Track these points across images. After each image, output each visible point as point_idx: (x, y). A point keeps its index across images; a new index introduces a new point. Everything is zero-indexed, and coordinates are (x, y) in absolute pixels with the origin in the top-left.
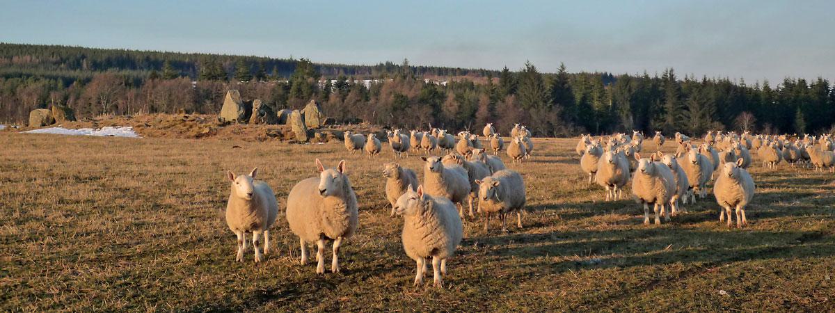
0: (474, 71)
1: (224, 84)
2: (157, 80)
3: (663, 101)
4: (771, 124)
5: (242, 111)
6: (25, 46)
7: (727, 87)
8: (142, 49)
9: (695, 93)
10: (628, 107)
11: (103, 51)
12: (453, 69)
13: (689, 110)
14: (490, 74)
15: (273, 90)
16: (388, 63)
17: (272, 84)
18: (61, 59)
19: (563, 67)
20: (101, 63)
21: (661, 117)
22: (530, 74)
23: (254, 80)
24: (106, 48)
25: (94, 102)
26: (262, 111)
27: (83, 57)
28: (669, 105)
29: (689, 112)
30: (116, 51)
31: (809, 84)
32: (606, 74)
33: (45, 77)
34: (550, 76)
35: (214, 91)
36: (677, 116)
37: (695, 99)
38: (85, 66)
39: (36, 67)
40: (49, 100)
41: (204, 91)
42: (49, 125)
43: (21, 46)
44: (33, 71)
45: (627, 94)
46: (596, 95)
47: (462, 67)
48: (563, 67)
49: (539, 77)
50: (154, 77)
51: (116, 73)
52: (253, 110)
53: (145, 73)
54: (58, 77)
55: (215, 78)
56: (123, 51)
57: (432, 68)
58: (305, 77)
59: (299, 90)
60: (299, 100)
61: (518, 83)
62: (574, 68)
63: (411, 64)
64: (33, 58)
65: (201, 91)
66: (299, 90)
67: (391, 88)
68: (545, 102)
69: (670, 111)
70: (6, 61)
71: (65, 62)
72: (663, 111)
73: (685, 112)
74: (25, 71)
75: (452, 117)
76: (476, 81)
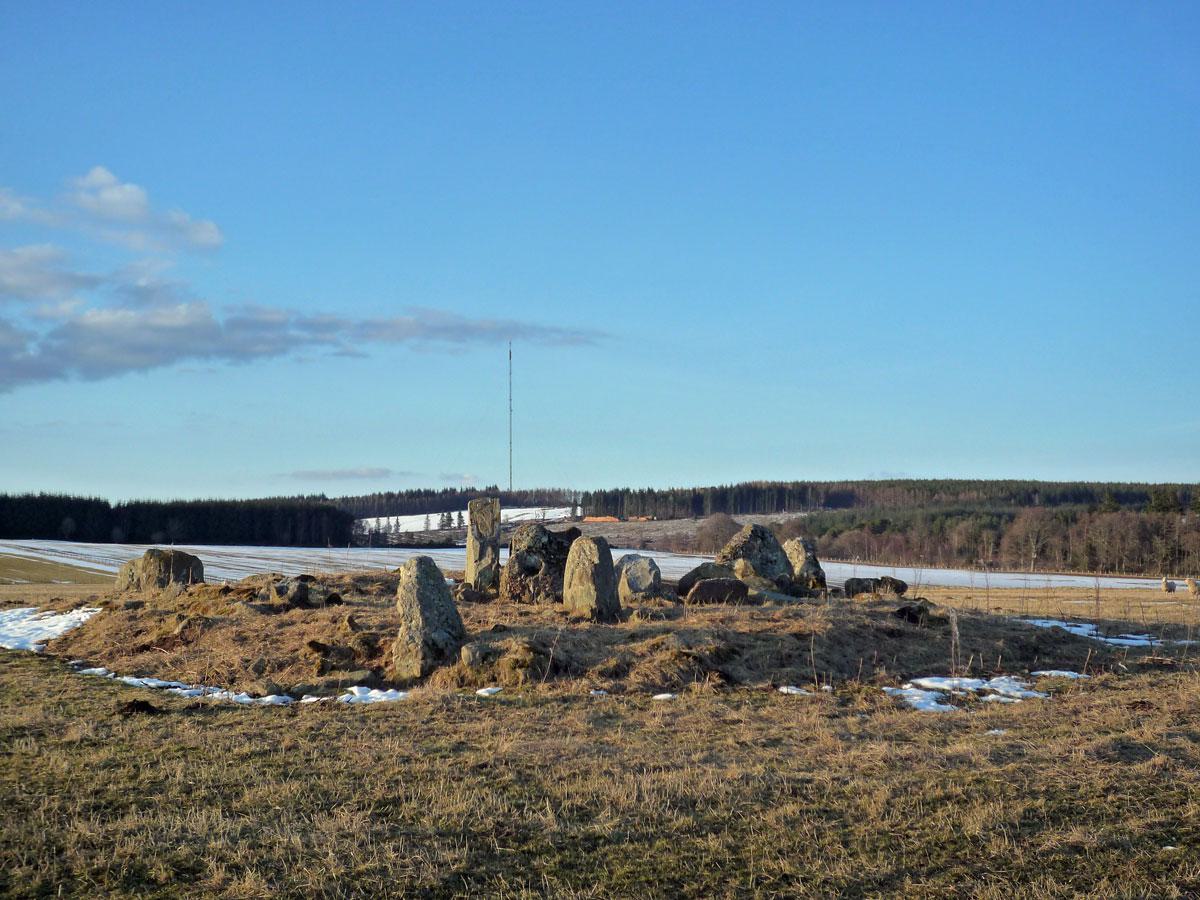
2: (1095, 514)
6: (974, 482)
8: (1104, 480)
11: (1058, 485)
18: (1011, 494)
20: (1055, 498)
25: (1021, 542)
26: (533, 559)
32: (419, 490)
33: (988, 514)
35: (1165, 525)
38: (1037, 501)
39: (982, 504)
40: (980, 539)
41: (1152, 525)
42: (1121, 571)
43: (969, 483)
44: (977, 508)
51: (1070, 508)
53: (1081, 509)
54: (1004, 514)
55: (1166, 509)
56: (1082, 483)
64: (981, 494)
65: (1148, 526)
70: (952, 498)
71: (1015, 497)
74: (969, 509)
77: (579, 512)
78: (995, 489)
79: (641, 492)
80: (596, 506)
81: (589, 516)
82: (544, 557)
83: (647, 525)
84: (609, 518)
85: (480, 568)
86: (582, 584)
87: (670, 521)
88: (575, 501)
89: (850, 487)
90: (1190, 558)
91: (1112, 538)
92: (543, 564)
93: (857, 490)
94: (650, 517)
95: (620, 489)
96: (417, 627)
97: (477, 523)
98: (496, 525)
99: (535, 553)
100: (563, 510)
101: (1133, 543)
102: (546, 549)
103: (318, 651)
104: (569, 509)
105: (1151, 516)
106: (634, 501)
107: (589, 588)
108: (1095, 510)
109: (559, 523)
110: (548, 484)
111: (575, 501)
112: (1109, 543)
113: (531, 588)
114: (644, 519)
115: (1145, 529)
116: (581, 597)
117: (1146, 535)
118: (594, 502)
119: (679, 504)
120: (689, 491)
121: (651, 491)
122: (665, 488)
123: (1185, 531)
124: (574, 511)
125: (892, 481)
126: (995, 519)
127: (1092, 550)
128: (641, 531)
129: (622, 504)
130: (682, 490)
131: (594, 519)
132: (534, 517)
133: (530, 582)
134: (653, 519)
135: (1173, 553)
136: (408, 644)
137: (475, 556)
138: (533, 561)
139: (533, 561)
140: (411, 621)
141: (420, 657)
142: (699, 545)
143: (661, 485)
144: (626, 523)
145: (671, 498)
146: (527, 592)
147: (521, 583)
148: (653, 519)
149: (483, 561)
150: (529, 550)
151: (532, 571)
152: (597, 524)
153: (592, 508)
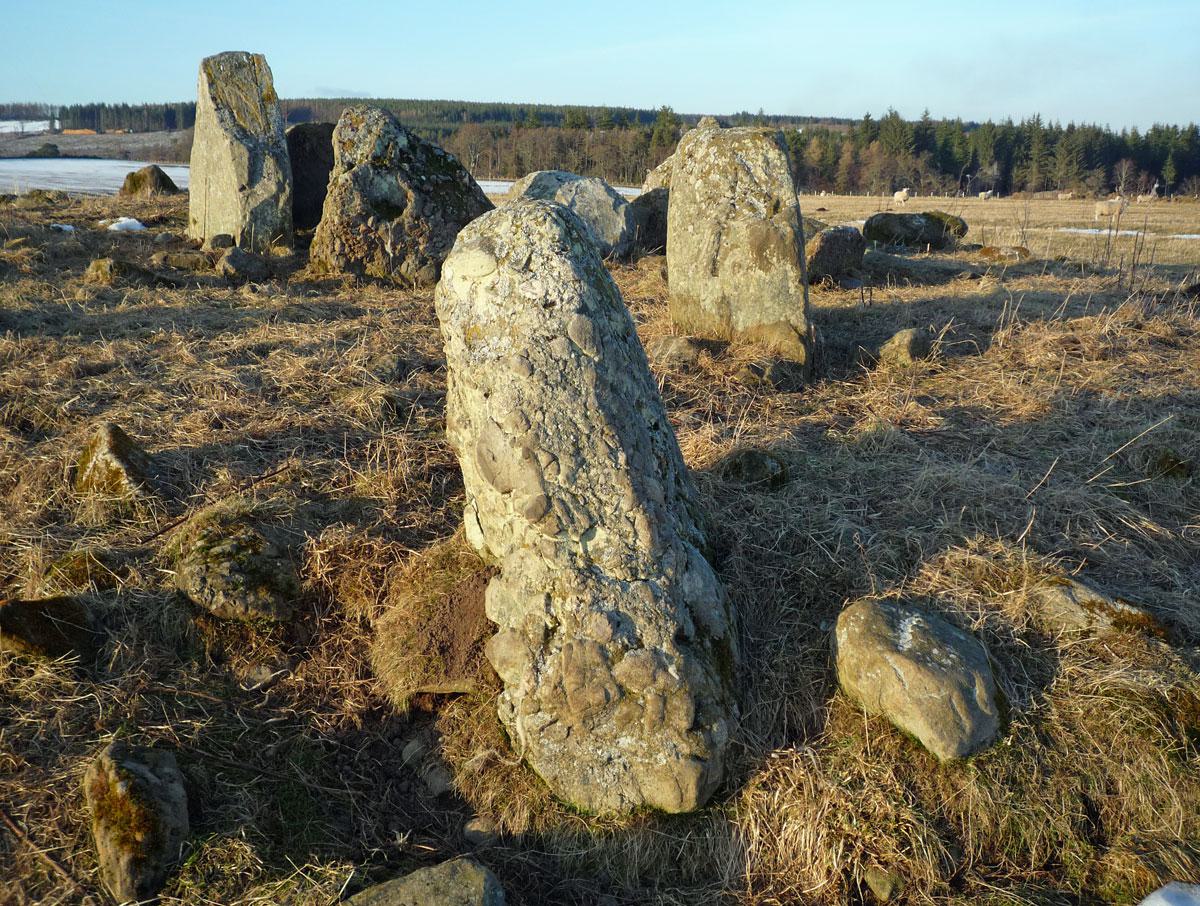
0: (826, 120)
1: (587, 133)
2: (522, 130)
3: (1028, 148)
4: (1147, 173)
5: (266, 188)
6: (412, 101)
7: (1096, 133)
9: (1062, 139)
10: (992, 154)
11: (481, 105)
12: (805, 118)
13: (1054, 156)
14: (852, 123)
15: (635, 138)
16: (744, 113)
17: (633, 132)
19: (927, 113)
21: (1025, 164)
22: (893, 122)
23: (616, 129)
24: (485, 101)
26: (389, 184)
27: (464, 110)
28: (1034, 152)
29: (981, 152)
30: (494, 104)
31: (1180, 129)
33: (427, 129)
34: (911, 124)
36: (1042, 163)
37: (1062, 146)
38: (465, 118)
39: (420, 120)
43: (408, 102)
44: (417, 124)
45: (991, 141)
46: (956, 142)
47: (814, 116)
48: (927, 113)
49: (903, 125)
50: (519, 127)
52: (333, 174)
53: (510, 126)
55: (578, 126)
56: (500, 104)
57: (786, 117)
58: (667, 124)
59: (661, 138)
60: (661, 149)
61: (879, 129)
62: (936, 116)
63: (765, 114)
65: (564, 139)
66: (661, 138)
67: (387, 630)
68: (907, 148)
69: (1035, 157)
71: (447, 115)
72: (1028, 157)
73: (1051, 158)
75: (814, 165)
76: (831, 129)
77: (57, 125)
78: (430, 108)
79: (116, 106)
80: (74, 119)
81: (67, 128)
82: (407, 177)
83: (125, 138)
84: (87, 131)
85: (253, 203)
86: (763, 262)
87: (147, 134)
88: (53, 115)
89: (307, 104)
90: (596, 167)
91: (535, 150)
92: (411, 194)
93: (313, 108)
94: (126, 130)
95: (96, 104)
96: (630, 556)
97: (227, 106)
98: (272, 109)
99: (389, 170)
100: (40, 123)
101: (553, 154)
102: (409, 161)
103: (51, 653)
104: (47, 122)
105: (567, 133)
106: (110, 114)
107: (785, 278)
108: (521, 126)
109: (39, 135)
110: (24, 98)
111: (53, 115)
112: (533, 155)
113: (388, 248)
114: (120, 131)
115: (562, 144)
116: (758, 300)
117: (563, 147)
118: (71, 116)
119: (153, 118)
120: (161, 106)
121: (125, 106)
122: (139, 104)
123: (593, 145)
124: (52, 125)
125: (343, 99)
126: (433, 133)
127: (519, 160)
128: (118, 143)
129: (99, 118)
130: (155, 105)
131: (72, 132)
132: (13, 130)
133: (385, 232)
134: (129, 132)
135: (583, 163)
136: (608, 661)
137: (240, 176)
138: (385, 186)
139: (385, 186)
140: (588, 534)
141: (682, 722)
142: (177, 155)
143: (135, 100)
144: (103, 136)
145: (145, 112)
146: (378, 254)
147: (366, 237)
148: (129, 132)
149: (258, 188)
150: (377, 161)
151: (386, 209)
152: (76, 136)
153: (70, 121)
